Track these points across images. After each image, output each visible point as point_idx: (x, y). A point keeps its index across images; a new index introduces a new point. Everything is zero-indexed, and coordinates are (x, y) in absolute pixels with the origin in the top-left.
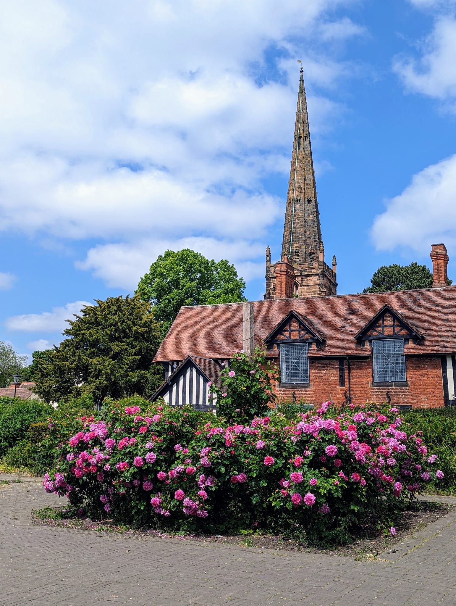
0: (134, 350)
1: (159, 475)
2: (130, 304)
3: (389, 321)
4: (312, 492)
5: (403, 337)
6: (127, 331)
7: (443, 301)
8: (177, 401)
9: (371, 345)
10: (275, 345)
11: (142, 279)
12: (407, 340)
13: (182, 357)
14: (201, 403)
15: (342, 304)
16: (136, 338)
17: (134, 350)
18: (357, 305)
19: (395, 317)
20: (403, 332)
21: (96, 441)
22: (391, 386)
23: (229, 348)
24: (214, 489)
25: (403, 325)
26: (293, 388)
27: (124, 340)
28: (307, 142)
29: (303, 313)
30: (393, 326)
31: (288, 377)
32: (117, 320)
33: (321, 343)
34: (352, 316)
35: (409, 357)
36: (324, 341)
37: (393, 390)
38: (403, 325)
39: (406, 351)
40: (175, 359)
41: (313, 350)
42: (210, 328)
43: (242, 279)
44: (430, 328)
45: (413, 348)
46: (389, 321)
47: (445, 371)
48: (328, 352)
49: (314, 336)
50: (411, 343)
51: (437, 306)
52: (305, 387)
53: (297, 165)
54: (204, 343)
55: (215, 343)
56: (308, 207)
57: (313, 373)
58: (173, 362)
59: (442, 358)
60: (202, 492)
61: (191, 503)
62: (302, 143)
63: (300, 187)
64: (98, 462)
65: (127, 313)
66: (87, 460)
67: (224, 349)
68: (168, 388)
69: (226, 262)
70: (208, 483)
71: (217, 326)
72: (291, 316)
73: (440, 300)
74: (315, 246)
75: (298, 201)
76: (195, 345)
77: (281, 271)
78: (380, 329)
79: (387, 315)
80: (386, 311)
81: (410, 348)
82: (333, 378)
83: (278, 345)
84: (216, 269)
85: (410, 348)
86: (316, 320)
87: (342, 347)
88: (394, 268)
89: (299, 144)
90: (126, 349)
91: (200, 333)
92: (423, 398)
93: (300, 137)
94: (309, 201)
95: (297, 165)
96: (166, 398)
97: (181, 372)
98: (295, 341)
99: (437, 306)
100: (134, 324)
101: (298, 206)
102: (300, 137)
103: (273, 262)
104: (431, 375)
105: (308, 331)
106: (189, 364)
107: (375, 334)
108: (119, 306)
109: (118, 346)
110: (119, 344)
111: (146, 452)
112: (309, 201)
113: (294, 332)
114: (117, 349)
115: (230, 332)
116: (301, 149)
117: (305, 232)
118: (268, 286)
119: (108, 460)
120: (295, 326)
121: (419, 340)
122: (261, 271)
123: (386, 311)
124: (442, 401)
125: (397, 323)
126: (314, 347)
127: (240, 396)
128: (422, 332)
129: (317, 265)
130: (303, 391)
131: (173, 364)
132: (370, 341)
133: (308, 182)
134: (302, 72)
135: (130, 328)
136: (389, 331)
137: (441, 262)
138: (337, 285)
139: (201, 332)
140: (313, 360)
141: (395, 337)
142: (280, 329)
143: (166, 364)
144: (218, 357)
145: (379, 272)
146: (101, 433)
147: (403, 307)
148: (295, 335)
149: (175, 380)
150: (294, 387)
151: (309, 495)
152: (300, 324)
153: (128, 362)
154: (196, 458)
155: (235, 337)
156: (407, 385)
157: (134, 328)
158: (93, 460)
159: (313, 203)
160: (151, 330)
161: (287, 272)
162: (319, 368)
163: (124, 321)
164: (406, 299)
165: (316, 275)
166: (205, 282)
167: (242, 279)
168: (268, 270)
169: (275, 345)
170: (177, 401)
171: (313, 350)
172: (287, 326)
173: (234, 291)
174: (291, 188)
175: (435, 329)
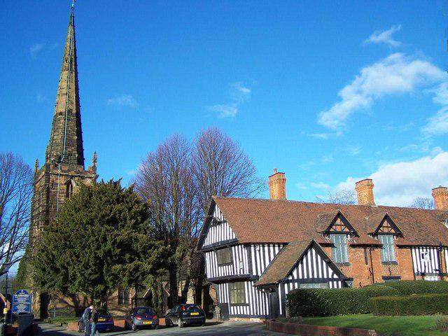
121: (355, 234)
165: (91, 178)
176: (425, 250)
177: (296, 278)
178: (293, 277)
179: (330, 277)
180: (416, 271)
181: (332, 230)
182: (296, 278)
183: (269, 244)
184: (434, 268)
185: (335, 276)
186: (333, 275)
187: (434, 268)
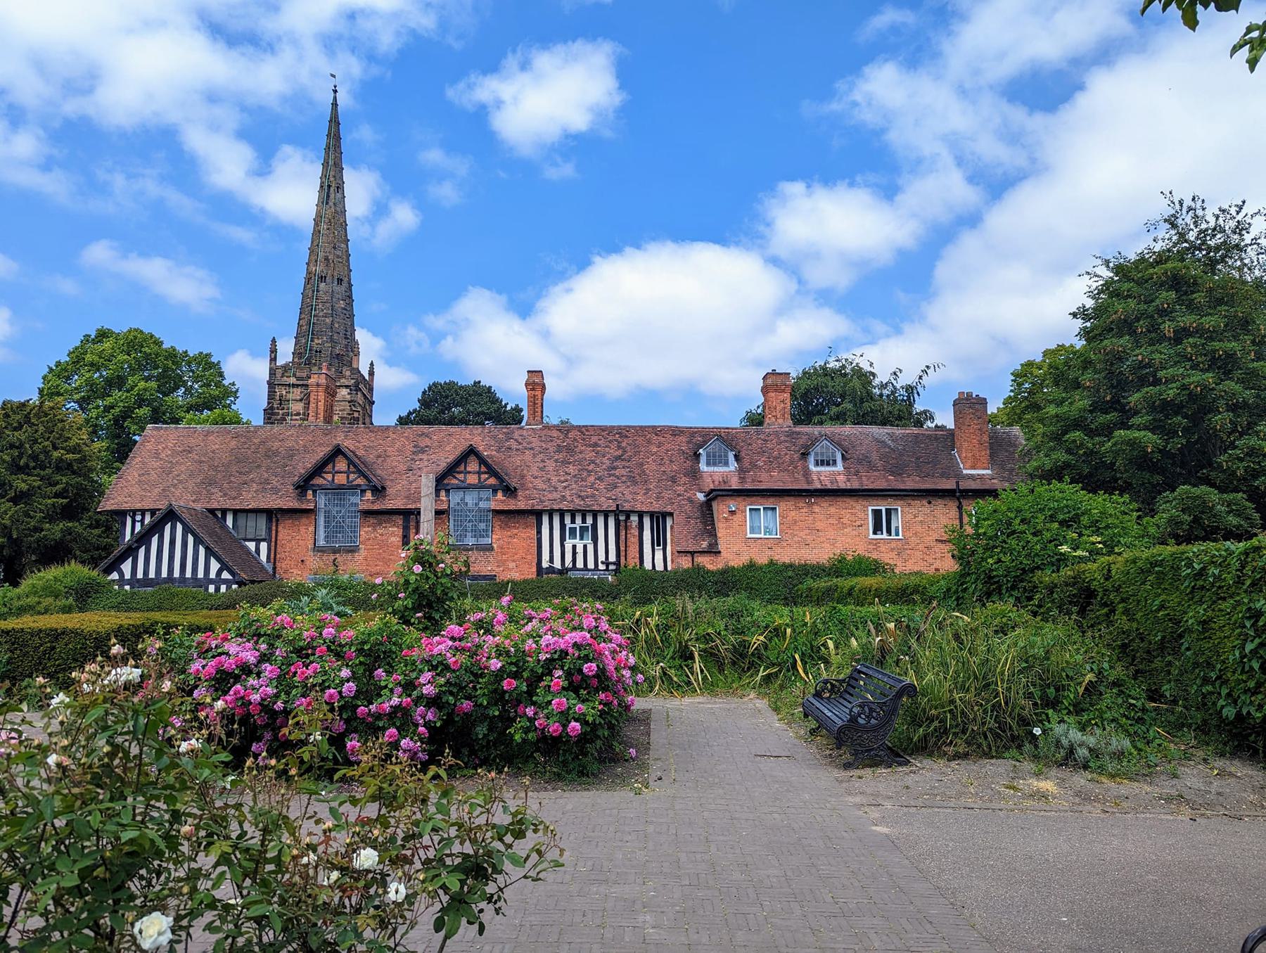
0: (54, 489)
1: (359, 710)
2: (46, 415)
3: (473, 465)
4: (576, 720)
5: (490, 487)
6: (42, 457)
7: (539, 443)
8: (146, 572)
9: (448, 495)
10: (310, 492)
11: (51, 369)
12: (495, 491)
13: (162, 505)
14: (188, 574)
15: (407, 438)
16: (58, 469)
17: (54, 489)
18: (427, 442)
19: (482, 461)
20: (492, 481)
21: (246, 670)
22: (472, 549)
23: (234, 494)
24: (438, 725)
25: (492, 472)
26: (335, 552)
27: (36, 472)
28: (339, 195)
29: (352, 448)
30: (479, 473)
31: (326, 537)
32: (23, 438)
33: (379, 491)
34: (420, 456)
35: (497, 512)
36: (384, 488)
37: (473, 555)
38: (492, 472)
39: (493, 505)
40: (138, 506)
41: (367, 501)
42: (201, 462)
43: (233, 384)
44: (523, 477)
45: (502, 502)
46: (473, 465)
47: (539, 532)
48: (390, 505)
49: (370, 481)
50: (500, 495)
51: (532, 449)
52: (353, 550)
53: (323, 226)
54: (191, 485)
55: (210, 485)
56: (337, 288)
57: (365, 532)
58: (134, 512)
59: (538, 514)
60: (421, 729)
61: (411, 744)
62: (332, 196)
63: (327, 259)
64: (263, 699)
65: (41, 428)
66: (242, 698)
67: (225, 495)
68: (131, 552)
69: (209, 355)
70: (430, 716)
71: (212, 459)
72: (337, 452)
73: (536, 443)
74: (346, 346)
75: (322, 278)
76: (175, 486)
77: (318, 385)
78: (461, 476)
79: (472, 458)
80: (471, 452)
81: (499, 501)
82: (393, 539)
83: (314, 492)
84: (189, 364)
85: (499, 501)
86: (371, 458)
87: (407, 497)
88: (451, 385)
89: (328, 196)
90: (39, 488)
91: (183, 468)
92: (512, 565)
93: (329, 186)
94: (340, 281)
95: (323, 226)
96: (126, 567)
97: (157, 528)
98: (341, 487)
99: (532, 449)
100: (55, 448)
101: (322, 285)
102: (329, 186)
103: (280, 362)
104: (522, 536)
105: (362, 474)
106: (171, 516)
107: (455, 481)
108: (27, 416)
109: (24, 481)
110: (25, 477)
111: (342, 683)
112: (340, 281)
113: (340, 474)
114: (24, 487)
115: (234, 469)
116: (331, 204)
117: (332, 324)
118: (271, 396)
119: (277, 696)
120: (341, 465)
121: (510, 491)
122: (261, 370)
123: (471, 452)
124: (534, 569)
125: (483, 469)
126: (369, 495)
127: (421, 595)
128: (514, 483)
129: (348, 373)
130: (349, 556)
131: (134, 514)
132: (448, 491)
133: (339, 253)
134: (335, 91)
135: (46, 453)
136: (472, 479)
137: (538, 393)
138: (373, 403)
139: (184, 467)
140: (367, 513)
141: (480, 487)
142: (319, 470)
143: (122, 514)
144: (215, 505)
145: (430, 388)
146: (250, 657)
147: (489, 447)
148: (341, 479)
149: (143, 539)
150: (335, 551)
151: (573, 724)
152: (350, 462)
153: (43, 508)
154: (409, 686)
155: (245, 478)
156: (492, 549)
157: (56, 454)
158: (255, 697)
159: (345, 284)
160: (84, 459)
161: (327, 387)
162: (374, 526)
163: (35, 441)
164: (495, 437)
166: (169, 382)
167: (233, 384)
168: (272, 372)
169: (310, 492)
170: (146, 572)
171: (367, 501)
172: (330, 466)
173: (215, 397)
174: (313, 258)
175: (529, 478)
176: (579, 520)
177: (128, 576)
178: (121, 574)
179: (213, 575)
180: (545, 564)
181: (318, 481)
182: (128, 576)
183: (606, 515)
184: (602, 557)
185: (226, 575)
186: (219, 573)
187: (602, 557)
